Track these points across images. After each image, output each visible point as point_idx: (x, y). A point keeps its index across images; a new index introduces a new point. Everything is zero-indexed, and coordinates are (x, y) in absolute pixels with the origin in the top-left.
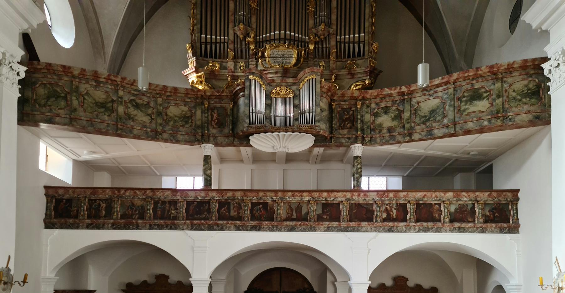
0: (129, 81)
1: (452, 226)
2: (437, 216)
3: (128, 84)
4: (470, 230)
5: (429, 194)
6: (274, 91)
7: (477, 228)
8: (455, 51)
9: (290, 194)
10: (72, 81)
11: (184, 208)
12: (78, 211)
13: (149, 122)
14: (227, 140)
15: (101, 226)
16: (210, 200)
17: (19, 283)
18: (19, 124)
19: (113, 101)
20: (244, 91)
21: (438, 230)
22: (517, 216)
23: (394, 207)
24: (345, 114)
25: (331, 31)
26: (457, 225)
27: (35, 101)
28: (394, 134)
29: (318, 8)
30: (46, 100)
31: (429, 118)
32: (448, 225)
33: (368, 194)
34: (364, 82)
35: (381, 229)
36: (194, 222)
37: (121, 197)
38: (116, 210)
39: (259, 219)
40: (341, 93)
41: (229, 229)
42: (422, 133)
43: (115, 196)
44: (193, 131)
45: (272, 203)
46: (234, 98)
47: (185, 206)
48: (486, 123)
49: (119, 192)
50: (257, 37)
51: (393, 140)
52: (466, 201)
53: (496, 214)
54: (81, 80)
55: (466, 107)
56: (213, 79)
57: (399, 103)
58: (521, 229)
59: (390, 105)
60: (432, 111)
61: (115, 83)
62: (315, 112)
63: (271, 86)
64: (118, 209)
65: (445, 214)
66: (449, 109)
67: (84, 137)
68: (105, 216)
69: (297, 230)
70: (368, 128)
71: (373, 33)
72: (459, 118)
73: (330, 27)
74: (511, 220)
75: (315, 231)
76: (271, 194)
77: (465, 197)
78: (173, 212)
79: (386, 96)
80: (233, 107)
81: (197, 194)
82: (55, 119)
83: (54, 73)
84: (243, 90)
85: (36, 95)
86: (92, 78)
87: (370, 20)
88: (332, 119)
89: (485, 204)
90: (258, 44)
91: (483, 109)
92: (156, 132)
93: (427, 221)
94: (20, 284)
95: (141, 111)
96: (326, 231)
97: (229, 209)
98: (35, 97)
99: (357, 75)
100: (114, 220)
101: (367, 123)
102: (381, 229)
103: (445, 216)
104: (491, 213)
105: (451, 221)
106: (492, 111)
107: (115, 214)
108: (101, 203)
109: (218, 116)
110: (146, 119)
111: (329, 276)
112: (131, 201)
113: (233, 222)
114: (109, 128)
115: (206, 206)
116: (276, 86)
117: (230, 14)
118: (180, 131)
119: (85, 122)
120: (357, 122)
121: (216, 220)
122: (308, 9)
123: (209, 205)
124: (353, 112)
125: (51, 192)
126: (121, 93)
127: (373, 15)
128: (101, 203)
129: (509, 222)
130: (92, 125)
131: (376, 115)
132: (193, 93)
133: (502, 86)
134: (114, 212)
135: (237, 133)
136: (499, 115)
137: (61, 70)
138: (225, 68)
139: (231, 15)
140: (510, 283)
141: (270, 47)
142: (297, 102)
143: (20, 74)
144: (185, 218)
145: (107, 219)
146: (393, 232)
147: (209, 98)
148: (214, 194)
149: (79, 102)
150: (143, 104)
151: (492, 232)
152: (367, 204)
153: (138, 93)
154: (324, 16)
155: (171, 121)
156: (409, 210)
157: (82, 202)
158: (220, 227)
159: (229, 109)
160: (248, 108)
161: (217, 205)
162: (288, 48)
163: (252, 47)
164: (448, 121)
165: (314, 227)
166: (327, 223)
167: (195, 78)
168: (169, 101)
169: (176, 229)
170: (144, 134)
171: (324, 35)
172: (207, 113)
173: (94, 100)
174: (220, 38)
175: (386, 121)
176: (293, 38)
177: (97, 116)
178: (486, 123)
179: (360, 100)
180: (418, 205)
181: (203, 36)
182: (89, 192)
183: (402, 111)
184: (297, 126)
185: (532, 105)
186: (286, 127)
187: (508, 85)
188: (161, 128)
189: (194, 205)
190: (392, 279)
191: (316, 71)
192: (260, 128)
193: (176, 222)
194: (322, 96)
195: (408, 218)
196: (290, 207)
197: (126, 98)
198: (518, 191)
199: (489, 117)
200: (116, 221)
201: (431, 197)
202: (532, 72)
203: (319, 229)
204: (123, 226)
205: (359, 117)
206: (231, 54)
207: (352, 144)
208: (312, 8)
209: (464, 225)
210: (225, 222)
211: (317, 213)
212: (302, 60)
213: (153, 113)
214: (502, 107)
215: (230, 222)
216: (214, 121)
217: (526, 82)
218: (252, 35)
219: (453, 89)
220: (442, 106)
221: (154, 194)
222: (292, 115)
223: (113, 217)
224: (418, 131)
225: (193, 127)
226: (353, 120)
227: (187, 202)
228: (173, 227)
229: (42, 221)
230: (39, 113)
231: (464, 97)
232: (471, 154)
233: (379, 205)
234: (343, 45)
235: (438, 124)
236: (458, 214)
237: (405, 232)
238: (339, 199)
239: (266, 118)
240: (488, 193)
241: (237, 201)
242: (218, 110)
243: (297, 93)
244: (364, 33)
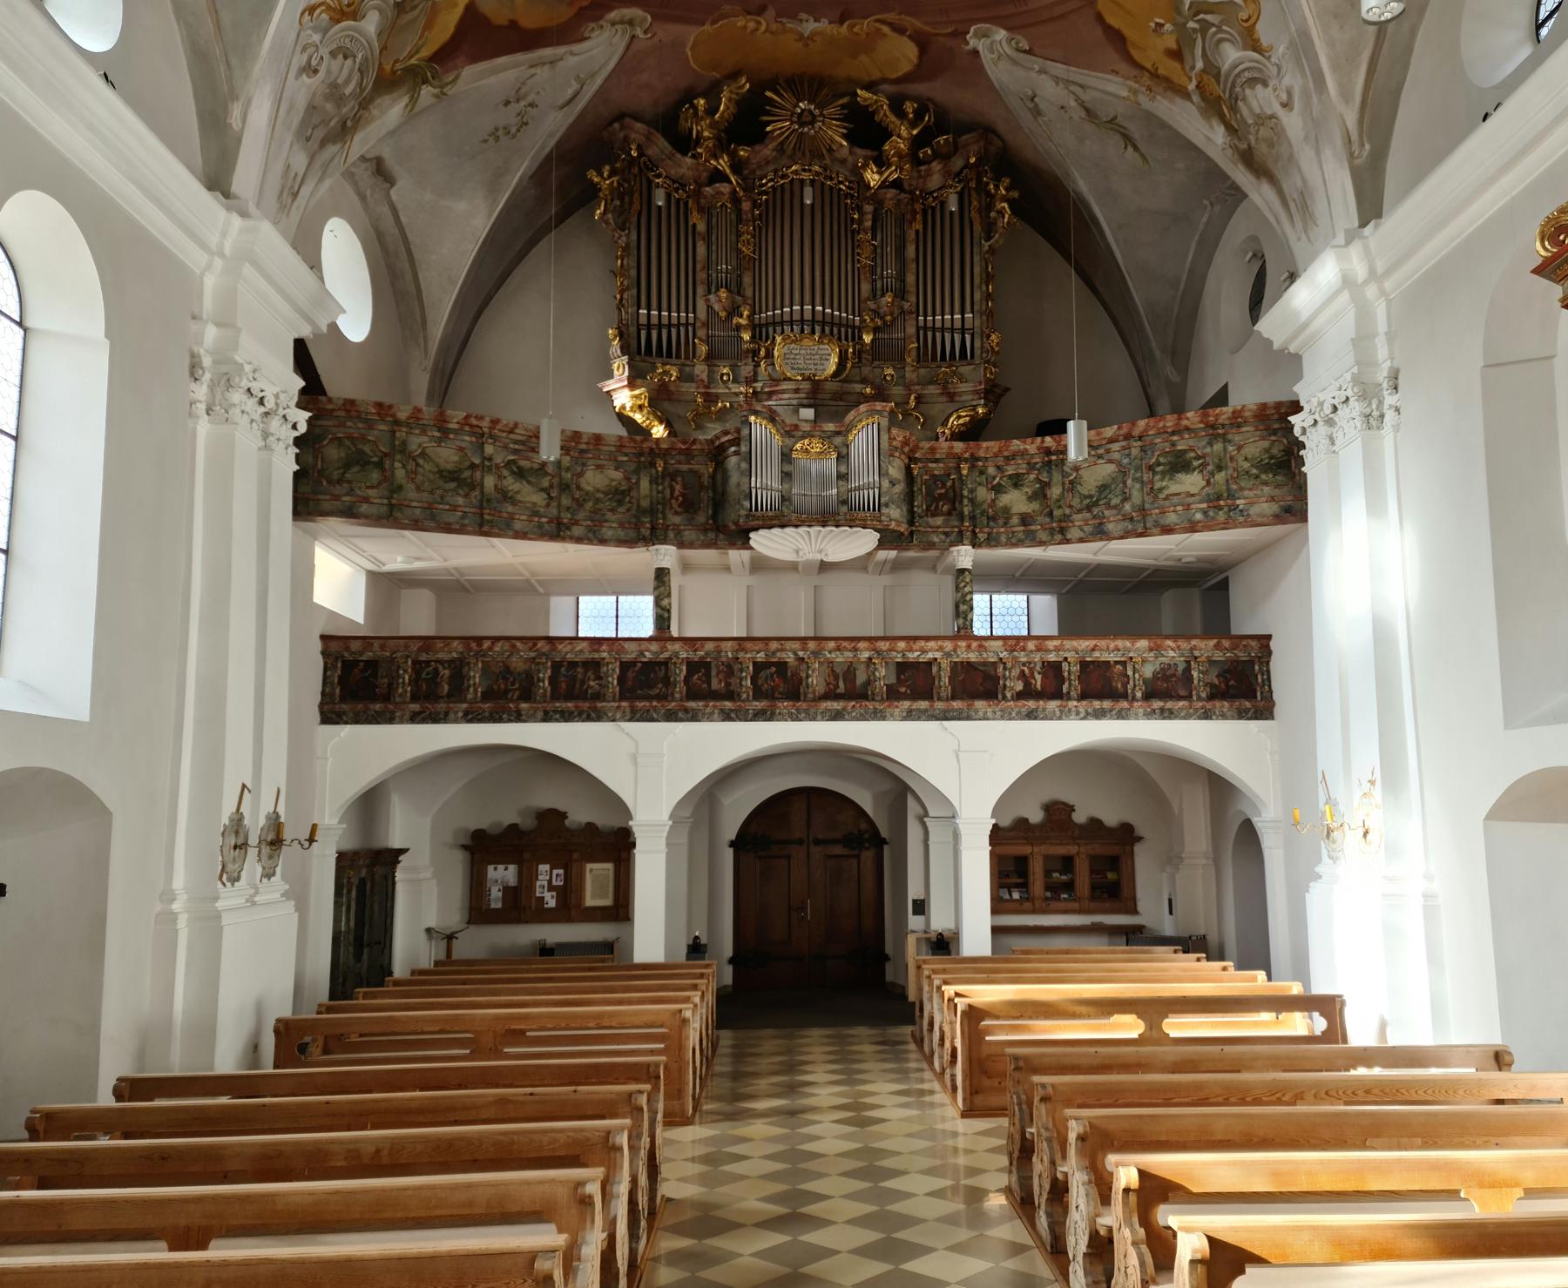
0: (506, 425)
1: (1149, 706)
2: (1119, 686)
3: (504, 431)
4: (1182, 714)
5: (1103, 643)
6: (798, 446)
7: (1196, 710)
8: (1154, 344)
9: (832, 644)
10: (394, 432)
11: (615, 676)
12: (390, 685)
13: (544, 503)
14: (702, 538)
15: (442, 716)
16: (670, 658)
17: (300, 843)
18: (294, 520)
19: (473, 466)
20: (738, 445)
21: (1121, 716)
22: (1270, 686)
23: (1038, 668)
24: (937, 485)
25: (906, 306)
26: (1157, 704)
27: (321, 472)
28: (1033, 528)
29: (879, 261)
30: (342, 471)
31: (1098, 500)
32: (1140, 704)
33: (986, 644)
34: (974, 410)
35: (1014, 714)
36: (638, 704)
37: (484, 656)
38: (471, 682)
39: (771, 696)
40: (928, 446)
41: (710, 718)
42: (1086, 528)
43: (472, 654)
44: (633, 520)
45: (797, 663)
46: (717, 454)
47: (618, 670)
48: (1199, 516)
49: (479, 645)
50: (755, 314)
51: (1032, 540)
52: (1173, 657)
53: (1232, 683)
54: (411, 428)
55: (1164, 484)
56: (664, 400)
57: (1042, 467)
58: (1277, 711)
59: (1024, 471)
60: (1102, 486)
61: (476, 429)
62: (880, 488)
63: (793, 437)
64: (477, 680)
65: (1134, 681)
66: (1133, 486)
67: (415, 539)
68: (449, 695)
69: (846, 717)
70: (982, 514)
71: (990, 314)
72: (1152, 503)
73: (903, 299)
74: (1259, 694)
75: (884, 718)
76: (793, 646)
77: (1172, 649)
78: (592, 683)
79: (1014, 456)
80: (715, 470)
81: (643, 647)
82: (360, 507)
83: (359, 417)
84: (736, 442)
85: (323, 461)
86: (432, 423)
87: (984, 288)
88: (913, 496)
89: (1211, 662)
90: (757, 330)
91: (1194, 490)
92: (559, 524)
93: (1100, 697)
94: (302, 845)
95: (528, 482)
96: (904, 719)
97: (708, 676)
98: (319, 466)
99: (960, 396)
100: (470, 703)
101: (981, 505)
102: (1014, 714)
103: (1135, 686)
104: (1222, 679)
105: (1148, 697)
106: (1208, 495)
107: (471, 690)
108: (440, 667)
109: (684, 489)
110: (538, 499)
111: (911, 803)
112: (503, 662)
113: (718, 704)
114: (466, 522)
115: (660, 670)
116: (803, 438)
117: (699, 267)
118: (607, 521)
119: (418, 512)
120: (961, 502)
121: (681, 700)
122: (859, 260)
123: (667, 667)
124: (954, 483)
125: (334, 647)
126: (489, 449)
127: (989, 278)
128: (440, 667)
129: (1256, 697)
130: (433, 517)
131: (998, 489)
132: (632, 444)
133: (1225, 449)
134: (469, 686)
135: (725, 526)
136: (1222, 503)
137: (374, 411)
138: (690, 378)
139: (701, 270)
140: (1263, 815)
141: (783, 339)
142: (843, 469)
143: (265, 401)
144: (617, 697)
145: (455, 702)
146: (1036, 718)
147: (665, 454)
148: (677, 646)
149: (407, 472)
150: (532, 468)
151: (1224, 717)
152: (985, 664)
153: (521, 447)
154: (892, 277)
155: (589, 500)
156: (1066, 674)
157: (399, 668)
158: (690, 715)
159: (706, 476)
160: (747, 480)
161: (684, 668)
162: (820, 342)
163: (746, 336)
164: (1133, 506)
165: (881, 711)
166: (906, 704)
167: (629, 399)
168: (584, 461)
169: (599, 719)
170: (536, 530)
171: (891, 314)
172: (662, 484)
173: (437, 466)
174: (679, 317)
175: (1016, 501)
176: (828, 319)
177: (442, 497)
178: (1199, 516)
179: (966, 460)
180: (1084, 665)
181: (643, 311)
182: (415, 646)
183: (1047, 485)
184: (846, 514)
185: (1277, 486)
186: (823, 514)
187: (1235, 447)
188: (569, 516)
189: (636, 669)
190: (1042, 808)
191: (879, 408)
192: (771, 518)
193: (599, 705)
194: (892, 455)
195: (1065, 690)
196: (833, 671)
197: (498, 460)
198: (1269, 637)
199: (1204, 505)
200: (474, 705)
201: (1108, 650)
202: (1276, 426)
203: (892, 715)
204: (487, 714)
205: (965, 493)
206: (703, 349)
207: (953, 544)
208: (866, 258)
209: (1169, 705)
210: (701, 704)
211: (887, 682)
212: (849, 365)
213: (551, 486)
214: (1224, 487)
215: (711, 704)
216: (677, 499)
217: (1266, 444)
218: (746, 313)
219: (1139, 449)
220: (1120, 479)
221: (554, 649)
222: (834, 491)
223: (465, 697)
224: (1077, 524)
225: (633, 512)
226: (954, 498)
227: (621, 662)
228: (593, 715)
229: (317, 709)
230: (328, 497)
231: (1159, 464)
232: (1183, 561)
233: (1009, 665)
234: (930, 334)
235: (1114, 512)
236: (1159, 683)
237: (1060, 718)
238: (930, 655)
239: (784, 499)
240: (1215, 641)
241: (724, 660)
242: (683, 478)
243: (844, 451)
244: (972, 312)
